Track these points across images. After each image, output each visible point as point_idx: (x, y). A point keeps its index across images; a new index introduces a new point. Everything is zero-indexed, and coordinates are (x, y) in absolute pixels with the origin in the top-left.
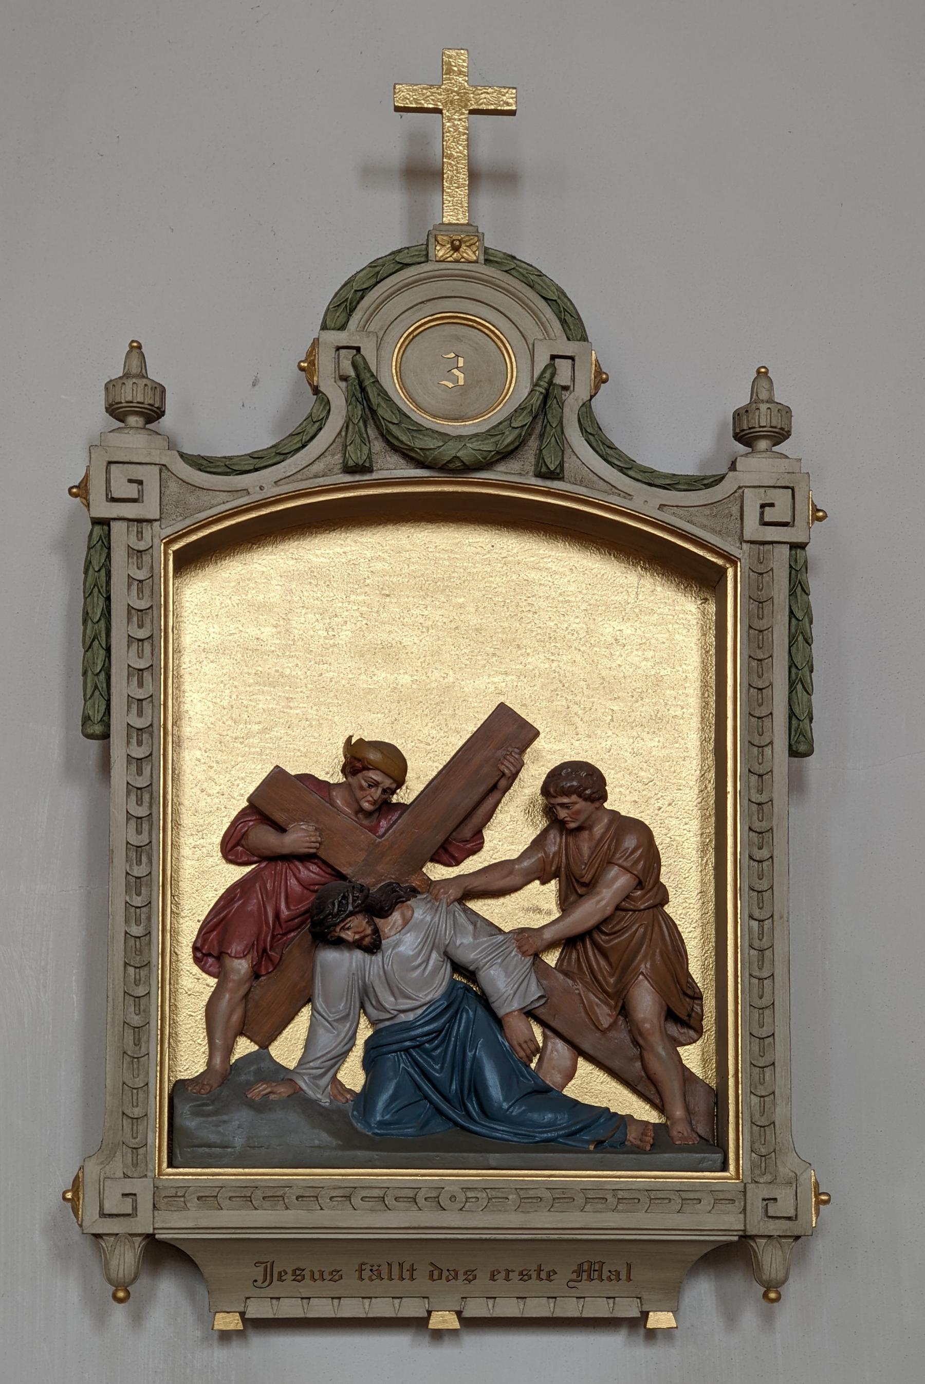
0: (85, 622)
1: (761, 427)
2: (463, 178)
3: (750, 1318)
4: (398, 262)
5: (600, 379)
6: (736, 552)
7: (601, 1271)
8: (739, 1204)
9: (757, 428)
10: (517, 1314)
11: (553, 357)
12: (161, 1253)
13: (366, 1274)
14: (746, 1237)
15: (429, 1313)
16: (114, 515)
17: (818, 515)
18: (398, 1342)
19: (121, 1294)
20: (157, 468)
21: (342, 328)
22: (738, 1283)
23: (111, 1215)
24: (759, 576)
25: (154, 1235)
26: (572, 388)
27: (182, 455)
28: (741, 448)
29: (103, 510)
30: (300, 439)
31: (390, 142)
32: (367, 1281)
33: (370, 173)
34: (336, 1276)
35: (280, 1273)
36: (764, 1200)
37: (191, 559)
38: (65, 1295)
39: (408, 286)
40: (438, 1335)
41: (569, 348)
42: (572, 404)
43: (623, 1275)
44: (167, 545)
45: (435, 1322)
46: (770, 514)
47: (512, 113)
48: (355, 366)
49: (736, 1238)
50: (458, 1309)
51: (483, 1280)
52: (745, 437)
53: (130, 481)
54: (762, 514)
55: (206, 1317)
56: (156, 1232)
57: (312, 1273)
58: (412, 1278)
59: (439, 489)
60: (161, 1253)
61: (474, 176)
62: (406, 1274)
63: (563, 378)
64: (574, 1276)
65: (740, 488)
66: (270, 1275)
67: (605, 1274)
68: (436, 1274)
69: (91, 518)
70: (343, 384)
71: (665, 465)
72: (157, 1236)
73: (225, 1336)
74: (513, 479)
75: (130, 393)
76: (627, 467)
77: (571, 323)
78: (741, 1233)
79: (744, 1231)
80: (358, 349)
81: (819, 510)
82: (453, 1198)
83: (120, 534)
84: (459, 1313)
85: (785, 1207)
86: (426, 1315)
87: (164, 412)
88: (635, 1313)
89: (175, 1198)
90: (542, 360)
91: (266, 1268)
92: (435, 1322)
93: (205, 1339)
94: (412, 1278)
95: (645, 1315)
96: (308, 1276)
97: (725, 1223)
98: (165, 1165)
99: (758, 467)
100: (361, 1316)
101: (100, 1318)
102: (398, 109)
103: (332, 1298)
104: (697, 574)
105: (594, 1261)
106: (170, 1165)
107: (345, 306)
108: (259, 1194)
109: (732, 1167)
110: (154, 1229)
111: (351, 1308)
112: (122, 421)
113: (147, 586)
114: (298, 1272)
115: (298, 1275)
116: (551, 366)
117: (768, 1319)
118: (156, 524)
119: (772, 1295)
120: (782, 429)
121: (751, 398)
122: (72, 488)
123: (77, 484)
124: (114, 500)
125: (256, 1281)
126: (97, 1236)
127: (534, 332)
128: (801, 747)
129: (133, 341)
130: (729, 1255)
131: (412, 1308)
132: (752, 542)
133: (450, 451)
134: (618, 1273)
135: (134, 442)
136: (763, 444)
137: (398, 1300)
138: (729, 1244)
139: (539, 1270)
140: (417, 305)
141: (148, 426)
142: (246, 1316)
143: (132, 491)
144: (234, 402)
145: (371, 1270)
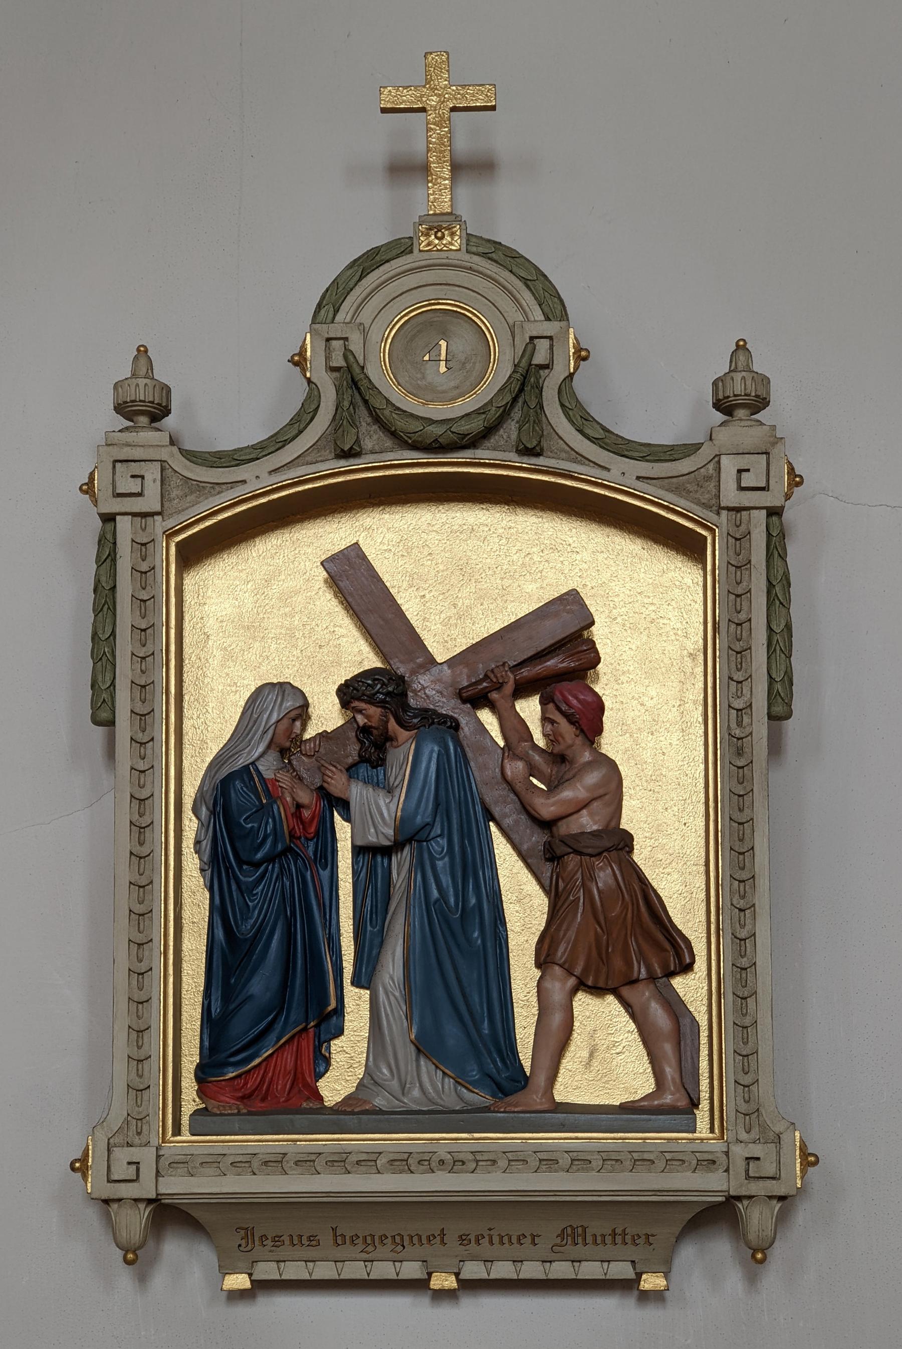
1: (735, 396)
5: (582, 356)
8: (164, 1163)
9: (741, 399)
10: (306, 1276)
14: (732, 1200)
15: (430, 1274)
16: (117, 511)
19: (130, 1256)
20: (158, 465)
24: (739, 539)
28: (719, 417)
29: (111, 506)
36: (747, 1158)
37: (197, 551)
38: (68, 1257)
40: (442, 1295)
41: (550, 328)
42: (551, 383)
46: (748, 480)
47: (493, 108)
49: (723, 1199)
50: (456, 1270)
53: (133, 476)
54: (739, 480)
56: (159, 1197)
59: (552, 479)
60: (167, 1215)
64: (559, 1240)
65: (716, 455)
66: (573, 1236)
71: (254, 433)
72: (163, 1201)
74: (491, 461)
75: (142, 392)
77: (553, 306)
80: (346, 339)
81: (796, 476)
82: (442, 1162)
84: (457, 1275)
86: (633, 1276)
88: (631, 1275)
89: (185, 1164)
90: (521, 342)
95: (639, 1275)
96: (287, 1242)
97: (713, 1184)
99: (742, 432)
102: (384, 111)
103: (278, 1261)
104: (688, 545)
107: (330, 302)
110: (158, 1195)
111: (324, 1271)
112: (132, 421)
113: (144, 576)
114: (277, 1239)
117: (752, 1279)
118: (158, 518)
119: (759, 1256)
120: (757, 396)
121: (730, 367)
122: (83, 485)
125: (240, 1246)
126: (106, 1202)
129: (142, 346)
132: (729, 509)
136: (741, 413)
137: (548, 1264)
138: (720, 1204)
141: (153, 425)
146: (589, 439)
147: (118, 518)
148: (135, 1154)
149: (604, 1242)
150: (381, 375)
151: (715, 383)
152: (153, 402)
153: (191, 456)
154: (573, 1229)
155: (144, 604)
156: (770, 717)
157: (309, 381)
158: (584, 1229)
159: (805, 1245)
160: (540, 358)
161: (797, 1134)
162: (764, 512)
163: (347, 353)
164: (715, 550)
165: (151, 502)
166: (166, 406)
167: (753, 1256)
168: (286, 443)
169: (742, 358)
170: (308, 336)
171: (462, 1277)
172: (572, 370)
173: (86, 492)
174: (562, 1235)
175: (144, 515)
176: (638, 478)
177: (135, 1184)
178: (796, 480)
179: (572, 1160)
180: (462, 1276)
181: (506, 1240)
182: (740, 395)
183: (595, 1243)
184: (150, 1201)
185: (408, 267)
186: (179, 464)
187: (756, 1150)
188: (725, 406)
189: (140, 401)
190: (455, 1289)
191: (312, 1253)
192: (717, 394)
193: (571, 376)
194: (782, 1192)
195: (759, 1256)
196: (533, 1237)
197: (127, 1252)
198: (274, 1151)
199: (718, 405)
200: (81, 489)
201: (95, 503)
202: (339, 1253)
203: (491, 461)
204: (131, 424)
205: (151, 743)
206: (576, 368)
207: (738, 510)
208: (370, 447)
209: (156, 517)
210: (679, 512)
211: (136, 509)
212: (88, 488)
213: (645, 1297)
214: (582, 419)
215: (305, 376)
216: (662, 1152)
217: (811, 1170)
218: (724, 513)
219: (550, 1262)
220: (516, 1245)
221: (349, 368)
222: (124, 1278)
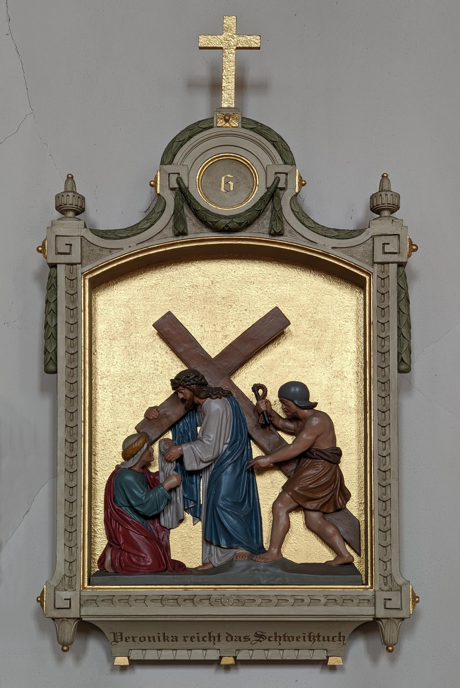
6: (371, 269)
12: (86, 628)
15: (328, 657)
18: (208, 673)
19: (65, 648)
21: (171, 163)
22: (376, 641)
25: (82, 618)
28: (57, 215)
29: (53, 259)
31: (203, 73)
35: (126, 638)
36: (384, 599)
37: (101, 282)
40: (227, 667)
45: (225, 661)
46: (388, 249)
47: (258, 48)
49: (372, 619)
50: (235, 655)
52: (376, 210)
53: (66, 244)
55: (111, 658)
60: (86, 628)
66: (260, 637)
68: (229, 638)
69: (48, 263)
72: (83, 619)
73: (123, 668)
74: (257, 235)
75: (70, 200)
76: (316, 228)
78: (373, 617)
79: (375, 615)
80: (179, 174)
83: (61, 271)
85: (395, 603)
89: (94, 600)
92: (225, 661)
94: (177, 641)
95: (221, 658)
97: (366, 612)
99: (381, 226)
100: (308, 659)
101: (60, 659)
104: (354, 281)
106: (89, 584)
110: (81, 616)
111: (182, 655)
112: (64, 214)
113: (73, 296)
116: (277, 180)
118: (79, 266)
123: (41, 245)
124: (387, 609)
127: (267, 161)
128: (404, 367)
129: (69, 174)
131: (319, 655)
135: (71, 227)
137: (267, 651)
139: (284, 636)
141: (76, 217)
142: (238, 658)
144: (117, 203)
146: (306, 227)
147: (58, 265)
148: (67, 594)
149: (333, 640)
150: (198, 194)
151: (372, 198)
152: (77, 206)
153: (96, 232)
155: (73, 310)
156: (400, 371)
158: (121, 634)
160: (281, 185)
162: (396, 265)
163: (179, 181)
164: (372, 284)
165: (75, 257)
166: (397, 206)
170: (159, 173)
171: (130, 658)
173: (40, 252)
175: (72, 264)
176: (333, 248)
177: (383, 608)
178: (413, 248)
180: (238, 658)
181: (151, 639)
182: (72, 205)
184: (78, 619)
185: (205, 137)
186: (91, 237)
187: (387, 595)
191: (175, 644)
193: (297, 194)
194: (401, 616)
196: (133, 638)
197: (63, 646)
201: (46, 258)
202: (189, 644)
203: (257, 235)
205: (76, 383)
207: (383, 263)
208: (193, 231)
211: (67, 261)
212: (42, 250)
214: (303, 217)
219: (298, 650)
220: (152, 642)
221: (180, 188)
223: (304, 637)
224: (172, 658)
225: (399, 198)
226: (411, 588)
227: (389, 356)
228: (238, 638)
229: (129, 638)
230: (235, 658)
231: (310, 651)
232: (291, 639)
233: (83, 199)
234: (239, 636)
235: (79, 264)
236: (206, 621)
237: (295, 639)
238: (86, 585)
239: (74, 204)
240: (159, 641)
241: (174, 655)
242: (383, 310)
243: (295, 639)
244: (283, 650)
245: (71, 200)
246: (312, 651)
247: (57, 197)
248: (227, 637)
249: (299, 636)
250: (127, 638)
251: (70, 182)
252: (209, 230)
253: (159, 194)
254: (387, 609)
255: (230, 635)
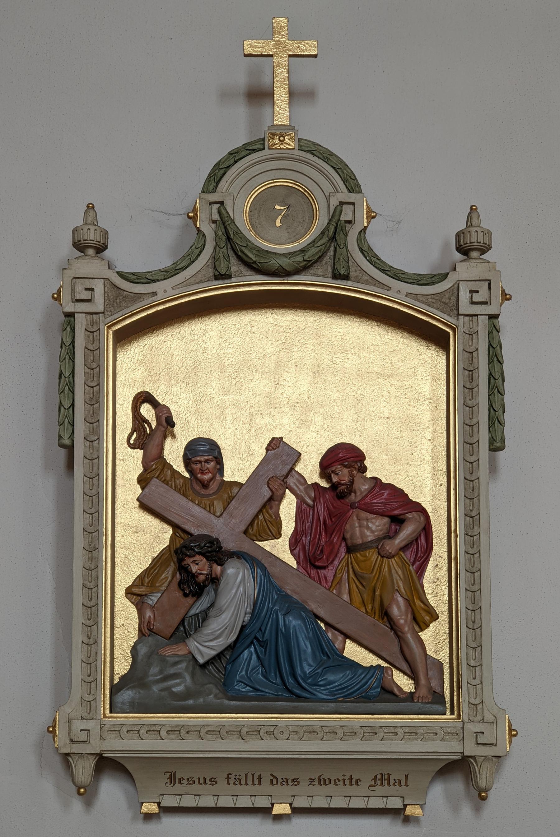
0: (60, 378)
1: (84, 240)
2: (285, 97)
3: (466, 810)
4: (249, 149)
7: (389, 780)
11: (342, 203)
13: (232, 781)
15: (273, 804)
17: (506, 297)
18: (383, 824)
20: (102, 280)
22: (457, 785)
23: (480, 744)
25: (102, 754)
26: (353, 222)
27: (119, 273)
28: (458, 256)
29: (69, 308)
30: (190, 258)
31: (240, 79)
32: (232, 785)
33: (225, 95)
34: (214, 781)
35: (180, 779)
36: (475, 733)
37: (125, 336)
39: (244, 171)
43: (403, 782)
44: (109, 328)
46: (477, 298)
47: (315, 56)
48: (219, 212)
49: (461, 758)
50: (158, 801)
51: (304, 784)
53: (86, 289)
57: (199, 779)
58: (260, 784)
60: (105, 764)
61: (291, 94)
62: (256, 782)
63: (347, 214)
67: (392, 782)
68: (275, 780)
69: (63, 312)
70: (213, 226)
72: (104, 755)
73: (148, 817)
75: (92, 236)
77: (353, 186)
79: (463, 753)
81: (506, 294)
83: (81, 322)
87: (107, 246)
88: (399, 805)
89: (117, 731)
90: (334, 202)
91: (171, 775)
93: (134, 818)
94: (260, 784)
96: (196, 782)
97: (450, 749)
98: (108, 711)
99: (467, 270)
102: (246, 55)
104: (437, 338)
105: (387, 772)
106: (111, 712)
108: (125, 729)
109: (456, 712)
112: (82, 252)
114: (296, 783)
115: (190, 781)
117: (478, 809)
124: (78, 301)
128: (496, 445)
129: (474, 206)
130: (458, 767)
133: (274, 263)
134: (400, 781)
135: (90, 266)
136: (474, 254)
138: (457, 761)
139: (351, 779)
140: (251, 179)
142: (161, 805)
143: (86, 295)
145: (235, 779)
151: (458, 235)
152: (99, 242)
154: (382, 774)
157: (198, 230)
158: (389, 775)
159: (503, 788)
161: (507, 716)
162: (487, 317)
166: (488, 245)
167: (85, 790)
168: (154, 281)
169: (474, 215)
172: (366, 224)
174: (375, 779)
179: (405, 733)
182: (93, 241)
183: (199, 783)
187: (479, 728)
188: (465, 251)
189: (91, 240)
190: (289, 814)
191: (214, 789)
192: (459, 241)
193: (365, 228)
195: (82, 790)
198: (132, 723)
199: (460, 249)
200: (53, 297)
204: (83, 254)
206: (368, 223)
209: (101, 314)
210: (438, 319)
211: (87, 310)
213: (407, 820)
215: (195, 225)
216: (361, 727)
217: (514, 738)
218: (461, 317)
222: (77, 805)
223: (344, 780)
224: (382, 806)
225: (491, 235)
226: (507, 721)
227: (480, 422)
228: (397, 781)
229: (184, 779)
230: (159, 804)
231: (365, 798)
232: (327, 782)
233: (107, 233)
234: (399, 780)
235: (101, 313)
236: (279, 758)
237: (332, 782)
238: (108, 715)
239: (88, 239)
240: (247, 784)
241: (310, 802)
242: (470, 372)
243: (332, 782)
244: (387, 797)
245: (92, 234)
246: (349, 798)
247: (75, 230)
248: (272, 780)
249: (359, 779)
250: (337, 781)
251: (91, 213)
252: (253, 273)
253: (199, 228)
254: (78, 301)
255: (275, 777)
